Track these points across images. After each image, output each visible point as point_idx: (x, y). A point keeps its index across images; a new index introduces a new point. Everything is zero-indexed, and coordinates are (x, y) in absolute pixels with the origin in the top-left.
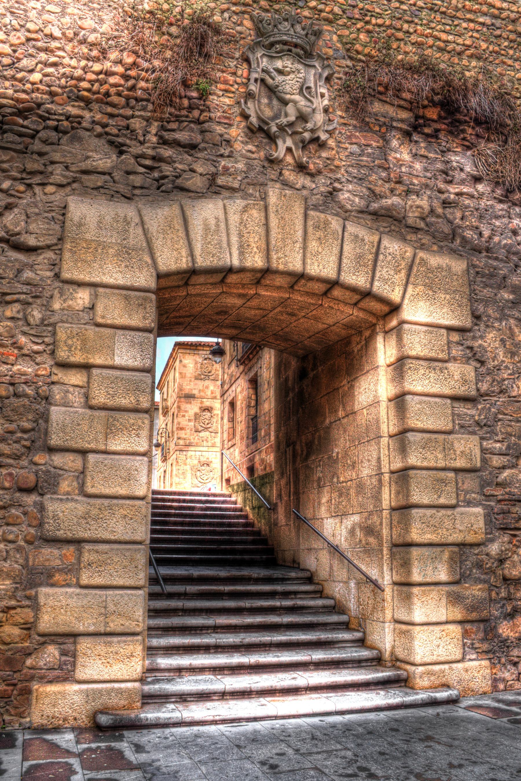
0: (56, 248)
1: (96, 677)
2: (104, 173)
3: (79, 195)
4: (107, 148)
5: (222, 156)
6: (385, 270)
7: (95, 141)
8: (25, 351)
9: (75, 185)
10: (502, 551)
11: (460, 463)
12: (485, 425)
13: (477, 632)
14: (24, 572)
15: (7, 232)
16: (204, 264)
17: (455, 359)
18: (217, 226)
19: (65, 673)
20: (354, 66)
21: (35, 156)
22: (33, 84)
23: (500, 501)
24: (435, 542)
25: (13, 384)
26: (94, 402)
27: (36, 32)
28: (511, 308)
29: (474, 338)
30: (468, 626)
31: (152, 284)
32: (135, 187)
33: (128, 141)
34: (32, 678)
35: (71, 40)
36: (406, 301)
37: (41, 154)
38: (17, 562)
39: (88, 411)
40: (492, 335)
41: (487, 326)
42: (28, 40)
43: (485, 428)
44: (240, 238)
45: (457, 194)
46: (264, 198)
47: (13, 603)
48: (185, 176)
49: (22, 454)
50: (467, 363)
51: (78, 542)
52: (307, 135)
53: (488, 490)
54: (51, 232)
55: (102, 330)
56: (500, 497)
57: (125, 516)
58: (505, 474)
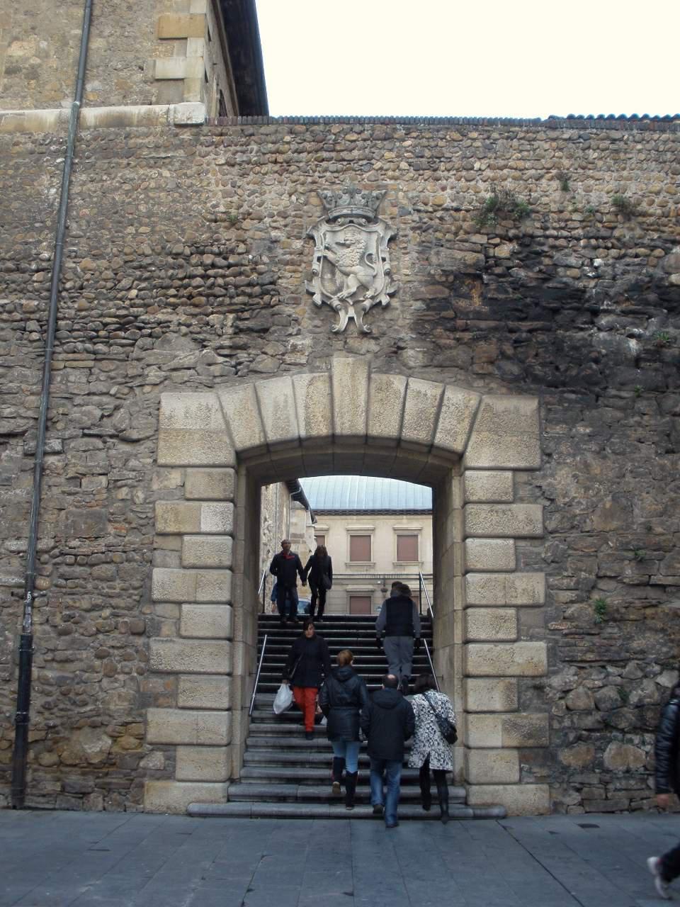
0: (154, 438)
1: (191, 777)
2: (189, 369)
3: (171, 391)
4: (192, 345)
5: (291, 335)
6: (448, 421)
8: (133, 525)
9: (166, 382)
10: (566, 683)
12: (552, 562)
14: (137, 695)
15: (116, 430)
16: (274, 438)
17: (522, 500)
18: (286, 401)
19: (167, 774)
20: (420, 219)
21: (135, 363)
22: (131, 299)
23: (566, 635)
24: (491, 674)
25: (125, 552)
26: (186, 563)
27: (131, 254)
28: (587, 441)
29: (544, 477)
30: (527, 752)
31: (231, 459)
32: (215, 377)
33: (208, 337)
34: (144, 775)
35: (159, 254)
36: (469, 449)
37: (138, 360)
38: (131, 689)
39: (182, 571)
40: (563, 472)
41: (559, 463)
42: (126, 262)
43: (553, 565)
44: (306, 410)
45: (530, 331)
47: (130, 719)
48: (258, 359)
49: (134, 606)
50: (535, 502)
51: (176, 673)
52: (367, 303)
54: (149, 426)
55: (191, 503)
56: (565, 632)
57: (211, 654)
58: (573, 609)
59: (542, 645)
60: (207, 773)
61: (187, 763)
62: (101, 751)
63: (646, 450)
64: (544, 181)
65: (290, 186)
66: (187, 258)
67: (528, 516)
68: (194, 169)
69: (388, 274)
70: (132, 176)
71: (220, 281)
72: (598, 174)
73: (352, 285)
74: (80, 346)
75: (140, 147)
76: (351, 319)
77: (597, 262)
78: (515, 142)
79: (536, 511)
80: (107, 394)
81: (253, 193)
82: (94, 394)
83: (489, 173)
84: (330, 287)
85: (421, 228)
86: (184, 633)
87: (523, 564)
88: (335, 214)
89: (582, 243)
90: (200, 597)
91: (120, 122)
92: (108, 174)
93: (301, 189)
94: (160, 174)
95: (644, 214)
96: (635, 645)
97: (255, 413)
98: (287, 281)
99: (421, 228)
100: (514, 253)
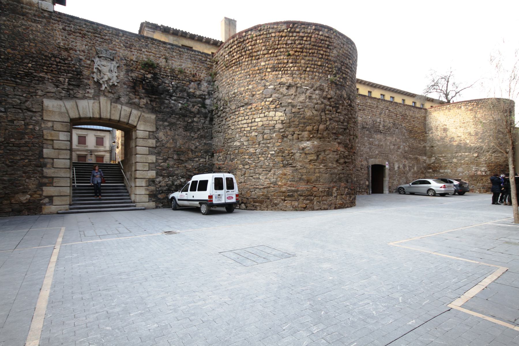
4: (53, 86)
7: (50, 84)
13: (150, 63)
17: (151, 139)
31: (68, 120)
37: (34, 87)
46: (99, 100)
51: (53, 178)
52: (111, 84)
53: (157, 167)
59: (155, 172)
60: (63, 203)
61: (56, 201)
62: (26, 199)
63: (181, 130)
64: (161, 59)
65: (85, 43)
66: (50, 58)
67: (152, 142)
68: (51, 28)
69: (117, 76)
70: (26, 23)
71: (62, 68)
73: (106, 78)
74: (9, 79)
75: (28, 13)
76: (106, 87)
77: (173, 83)
78: (154, 46)
79: (154, 141)
80: (22, 96)
81: (73, 42)
83: (146, 53)
84: (99, 77)
85: (126, 65)
87: (150, 153)
88: (101, 55)
89: (170, 77)
90: (60, 157)
92: (15, 20)
93: (89, 45)
94: (37, 26)
95: (185, 73)
96: (176, 172)
97: (76, 109)
98: (86, 72)
99: (126, 65)
100: (152, 77)
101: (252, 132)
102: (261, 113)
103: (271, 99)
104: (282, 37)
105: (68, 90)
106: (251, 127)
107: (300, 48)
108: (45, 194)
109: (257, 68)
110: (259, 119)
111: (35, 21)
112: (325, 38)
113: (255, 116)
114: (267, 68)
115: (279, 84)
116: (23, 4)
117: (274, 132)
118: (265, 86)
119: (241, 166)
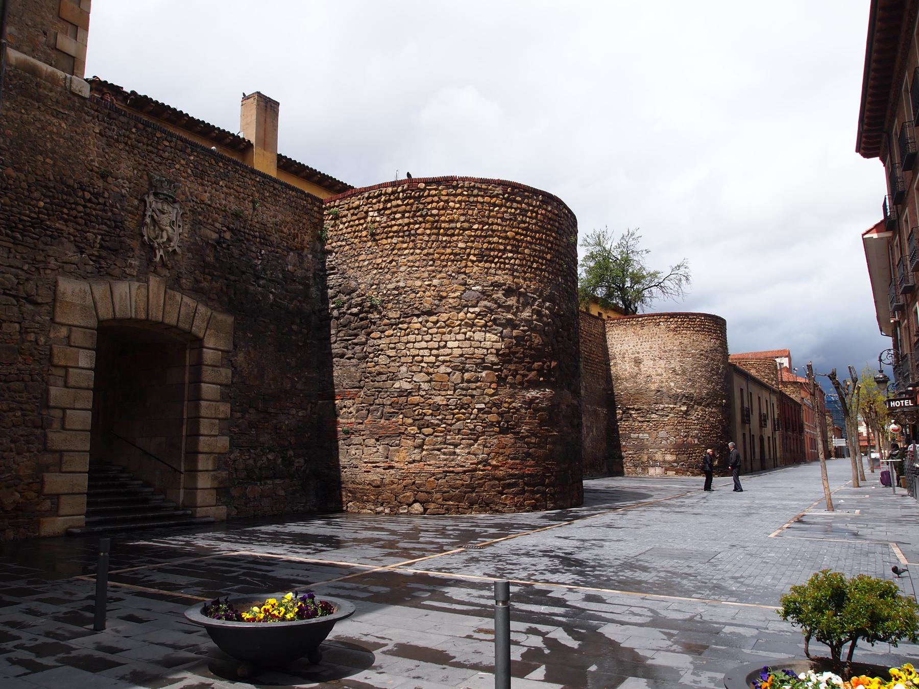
4: (75, 249)
11: (221, 416)
37: (43, 251)
46: (147, 282)
59: (227, 438)
61: (66, 505)
72: (268, 206)
82: (12, 267)
83: (225, 189)
84: (152, 235)
86: (67, 427)
90: (77, 406)
91: (34, 71)
92: (26, 110)
94: (60, 124)
97: (110, 300)
101: (438, 366)
102: (459, 333)
103: (477, 310)
104: (495, 205)
105: (98, 259)
106: (437, 356)
107: (523, 229)
108: (47, 490)
109: (449, 251)
110: (456, 344)
111: (57, 115)
112: (554, 217)
113: (447, 337)
114: (469, 255)
115: (492, 285)
116: (40, 77)
117: (485, 368)
118: (465, 284)
119: (413, 430)
